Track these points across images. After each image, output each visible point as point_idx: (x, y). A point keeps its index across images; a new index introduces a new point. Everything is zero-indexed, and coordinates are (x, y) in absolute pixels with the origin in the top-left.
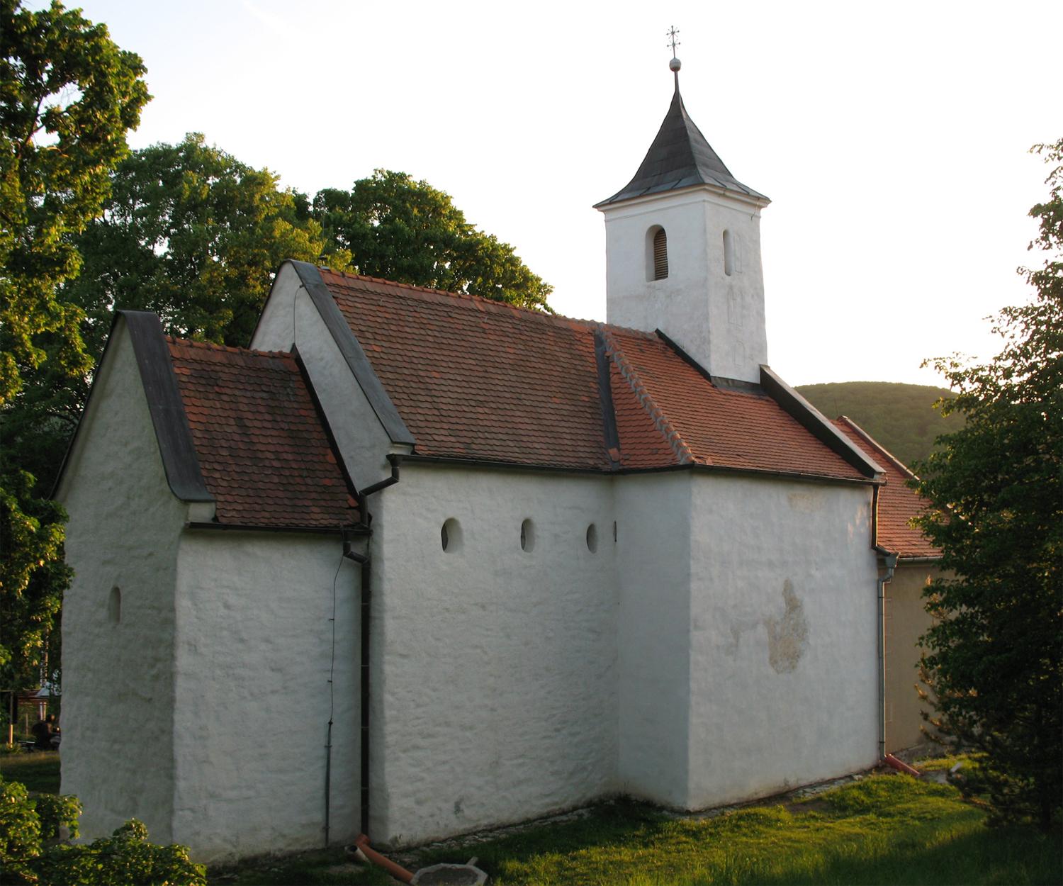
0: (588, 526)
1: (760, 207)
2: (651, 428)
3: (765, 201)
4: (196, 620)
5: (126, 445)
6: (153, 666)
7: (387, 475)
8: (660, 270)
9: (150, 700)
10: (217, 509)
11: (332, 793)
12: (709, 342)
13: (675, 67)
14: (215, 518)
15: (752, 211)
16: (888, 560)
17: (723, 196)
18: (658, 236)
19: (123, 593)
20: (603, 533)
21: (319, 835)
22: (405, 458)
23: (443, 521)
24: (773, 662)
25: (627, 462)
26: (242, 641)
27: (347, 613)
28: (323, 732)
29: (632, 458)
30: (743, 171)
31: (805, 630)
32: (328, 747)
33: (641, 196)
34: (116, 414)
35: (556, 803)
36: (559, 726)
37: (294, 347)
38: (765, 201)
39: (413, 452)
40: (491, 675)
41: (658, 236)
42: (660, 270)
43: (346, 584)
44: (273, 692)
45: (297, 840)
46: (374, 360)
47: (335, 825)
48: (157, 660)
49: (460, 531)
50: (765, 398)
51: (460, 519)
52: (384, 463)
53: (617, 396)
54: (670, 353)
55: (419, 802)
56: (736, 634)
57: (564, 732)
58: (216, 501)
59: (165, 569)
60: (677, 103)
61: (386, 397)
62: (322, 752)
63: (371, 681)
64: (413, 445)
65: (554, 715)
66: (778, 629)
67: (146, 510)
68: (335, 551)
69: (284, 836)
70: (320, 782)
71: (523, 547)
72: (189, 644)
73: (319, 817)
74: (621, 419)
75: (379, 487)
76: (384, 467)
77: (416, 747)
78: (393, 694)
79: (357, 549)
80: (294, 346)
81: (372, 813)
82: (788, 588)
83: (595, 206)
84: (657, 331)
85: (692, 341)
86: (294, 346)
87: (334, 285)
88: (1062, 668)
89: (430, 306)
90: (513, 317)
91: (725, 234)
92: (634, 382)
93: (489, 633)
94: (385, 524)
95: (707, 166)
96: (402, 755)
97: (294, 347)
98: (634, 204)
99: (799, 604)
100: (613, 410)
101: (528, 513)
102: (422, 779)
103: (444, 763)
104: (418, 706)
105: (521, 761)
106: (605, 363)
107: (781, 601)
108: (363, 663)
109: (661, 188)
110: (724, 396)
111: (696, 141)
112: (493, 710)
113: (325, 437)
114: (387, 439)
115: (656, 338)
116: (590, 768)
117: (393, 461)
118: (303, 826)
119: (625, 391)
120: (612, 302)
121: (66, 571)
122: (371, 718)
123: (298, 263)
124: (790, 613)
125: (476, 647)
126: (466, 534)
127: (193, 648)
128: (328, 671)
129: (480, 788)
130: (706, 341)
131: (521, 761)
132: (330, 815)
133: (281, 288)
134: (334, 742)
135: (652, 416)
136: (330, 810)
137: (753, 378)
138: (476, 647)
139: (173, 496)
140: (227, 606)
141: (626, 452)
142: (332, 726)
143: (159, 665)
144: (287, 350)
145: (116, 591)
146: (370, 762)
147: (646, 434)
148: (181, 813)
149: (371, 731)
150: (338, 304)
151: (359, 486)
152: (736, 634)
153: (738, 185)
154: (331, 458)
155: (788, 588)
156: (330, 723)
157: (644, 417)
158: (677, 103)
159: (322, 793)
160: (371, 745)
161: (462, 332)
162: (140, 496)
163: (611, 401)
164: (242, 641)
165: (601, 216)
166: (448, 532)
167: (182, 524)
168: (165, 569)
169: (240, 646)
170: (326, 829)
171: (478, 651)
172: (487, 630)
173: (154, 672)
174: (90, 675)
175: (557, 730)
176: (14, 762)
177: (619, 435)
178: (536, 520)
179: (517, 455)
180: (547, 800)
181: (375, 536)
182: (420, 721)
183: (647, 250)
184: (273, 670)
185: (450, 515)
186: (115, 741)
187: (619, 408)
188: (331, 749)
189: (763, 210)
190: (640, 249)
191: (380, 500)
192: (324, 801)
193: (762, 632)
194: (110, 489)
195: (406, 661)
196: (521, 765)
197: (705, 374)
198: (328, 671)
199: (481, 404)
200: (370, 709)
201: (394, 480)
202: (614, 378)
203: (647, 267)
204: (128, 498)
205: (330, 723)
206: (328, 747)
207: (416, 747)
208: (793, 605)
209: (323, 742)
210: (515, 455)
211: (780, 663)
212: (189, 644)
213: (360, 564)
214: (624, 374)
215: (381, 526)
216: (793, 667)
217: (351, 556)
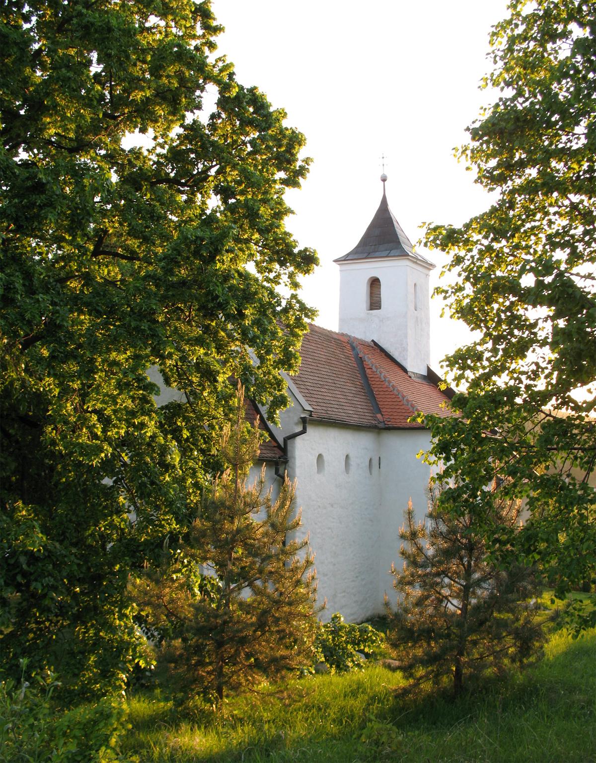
1: (430, 269)
2: (401, 404)
7: (299, 429)
8: (375, 303)
12: (407, 351)
17: (416, 263)
18: (375, 283)
25: (389, 423)
29: (392, 420)
33: (366, 258)
41: (375, 283)
42: (375, 303)
53: (373, 383)
54: (383, 354)
60: (384, 202)
64: (311, 411)
75: (294, 436)
76: (297, 424)
83: (335, 261)
85: (396, 349)
91: (415, 285)
92: (383, 374)
94: (297, 457)
100: (372, 391)
106: (360, 361)
109: (377, 254)
112: (334, 565)
114: (300, 408)
115: (372, 344)
117: (304, 421)
119: (378, 379)
120: (342, 321)
130: (405, 349)
135: (400, 396)
137: (425, 373)
158: (384, 202)
163: (369, 385)
165: (337, 267)
175: (357, 577)
181: (290, 463)
187: (376, 389)
191: (294, 443)
197: (405, 370)
199: (322, 386)
201: (304, 431)
202: (368, 371)
214: (374, 369)
215: (294, 458)
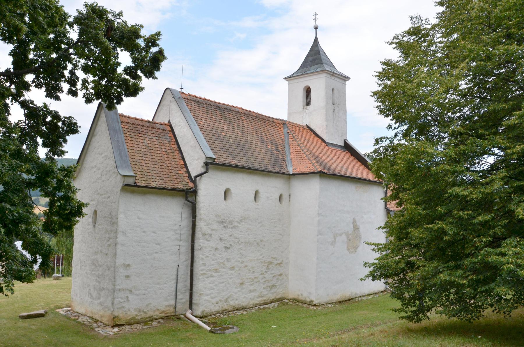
0: (280, 195)
3: (349, 78)
4: (126, 223)
5: (101, 154)
6: (108, 241)
7: (203, 170)
9: (107, 254)
11: (178, 293)
13: (316, 28)
14: (135, 183)
15: (343, 82)
16: (391, 213)
18: (308, 91)
20: (285, 197)
21: (172, 309)
22: (211, 164)
23: (225, 189)
24: (348, 249)
26: (144, 232)
27: (186, 223)
28: (176, 269)
30: (341, 68)
32: (177, 275)
35: (264, 300)
37: (169, 122)
38: (349, 78)
45: (163, 312)
46: (200, 127)
47: (179, 306)
48: (110, 238)
49: (231, 193)
51: (231, 189)
52: (203, 165)
54: (311, 133)
55: (212, 298)
56: (335, 238)
57: (268, 273)
59: (115, 202)
60: (316, 40)
61: (205, 141)
62: (175, 277)
64: (214, 159)
67: (108, 180)
68: (182, 201)
69: (158, 310)
70: (174, 289)
71: (255, 201)
72: (123, 232)
73: (173, 302)
81: (194, 302)
82: (354, 222)
83: (285, 79)
84: (306, 125)
87: (185, 98)
90: (253, 116)
91: (333, 89)
93: (241, 233)
95: (327, 64)
96: (206, 279)
97: (169, 122)
101: (257, 188)
102: (214, 289)
103: (222, 283)
111: (323, 56)
113: (180, 155)
118: (166, 306)
121: (71, 199)
126: (233, 195)
127: (124, 233)
129: (236, 293)
132: (177, 302)
133: (165, 98)
136: (177, 300)
139: (119, 175)
140: (139, 218)
143: (111, 240)
144: (166, 122)
147: (303, 161)
150: (187, 106)
152: (335, 238)
153: (338, 72)
154: (182, 163)
155: (354, 222)
156: (178, 266)
158: (316, 40)
159: (174, 293)
162: (106, 174)
164: (144, 232)
166: (226, 193)
167: (122, 185)
168: (115, 202)
169: (144, 234)
170: (175, 308)
173: (109, 243)
174: (84, 244)
178: (260, 191)
180: (261, 299)
183: (303, 95)
184: (156, 244)
185: (228, 187)
186: (93, 271)
189: (347, 82)
190: (301, 95)
192: (175, 297)
193: (344, 237)
194: (95, 172)
195: (209, 242)
196: (252, 285)
200: (194, 260)
203: (303, 101)
204: (102, 175)
205: (178, 266)
206: (177, 275)
207: (212, 276)
208: (356, 228)
209: (175, 273)
210: (255, 165)
212: (123, 232)
216: (356, 252)
217: (189, 201)
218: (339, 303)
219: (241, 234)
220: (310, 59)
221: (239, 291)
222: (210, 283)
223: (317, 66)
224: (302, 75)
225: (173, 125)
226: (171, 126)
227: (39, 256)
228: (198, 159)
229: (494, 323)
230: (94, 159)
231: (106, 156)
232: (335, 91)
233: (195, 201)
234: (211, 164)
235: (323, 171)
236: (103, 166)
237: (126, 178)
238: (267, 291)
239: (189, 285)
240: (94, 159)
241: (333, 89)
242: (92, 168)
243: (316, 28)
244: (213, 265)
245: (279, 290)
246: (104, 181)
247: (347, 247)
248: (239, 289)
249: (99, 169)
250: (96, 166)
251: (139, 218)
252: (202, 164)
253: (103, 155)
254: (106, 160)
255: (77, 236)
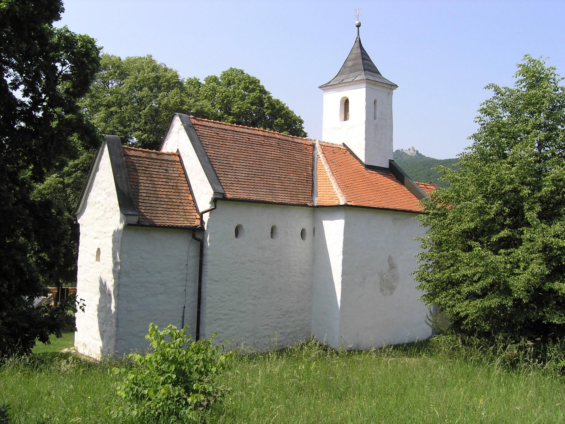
5: (105, 190)
10: (139, 218)
14: (138, 222)
18: (346, 103)
19: (101, 251)
20: (309, 232)
22: (220, 199)
24: (382, 290)
26: (148, 272)
27: (194, 262)
31: (398, 278)
32: (183, 317)
34: (101, 177)
36: (284, 313)
37: (178, 151)
38: (396, 86)
39: (223, 197)
40: (254, 290)
43: (193, 249)
44: (161, 294)
50: (390, 174)
53: (320, 173)
58: (138, 215)
62: (181, 319)
63: (202, 290)
65: (282, 309)
66: (385, 276)
71: (272, 237)
74: (320, 183)
77: (220, 319)
78: (210, 296)
79: (198, 236)
80: (178, 150)
82: (390, 258)
86: (178, 150)
88: (564, 257)
89: (238, 133)
97: (178, 151)
98: (339, 87)
99: (396, 266)
104: (222, 302)
105: (266, 327)
107: (387, 265)
108: (199, 283)
110: (370, 174)
116: (298, 332)
122: (201, 306)
123: (183, 115)
124: (390, 270)
125: (248, 278)
128: (184, 286)
131: (266, 327)
134: (186, 316)
138: (248, 278)
140: (143, 258)
141: (320, 198)
142: (185, 308)
144: (175, 151)
145: (99, 251)
146: (200, 324)
148: (120, 341)
149: (201, 311)
151: (201, 210)
155: (390, 258)
156: (184, 307)
157: (329, 183)
160: (201, 317)
161: (251, 145)
162: (109, 212)
164: (148, 272)
171: (249, 280)
172: (253, 271)
175: (284, 315)
176: (343, 198)
177: (318, 190)
179: (270, 198)
182: (222, 308)
185: (240, 223)
188: (185, 318)
198: (184, 286)
200: (201, 302)
205: (184, 307)
206: (183, 317)
207: (220, 319)
208: (392, 266)
209: (181, 315)
211: (385, 291)
213: (200, 243)
216: (392, 293)
218: (406, 350)
219: (254, 274)
220: (350, 64)
221: (251, 335)
222: (218, 327)
223: (357, 72)
224: (339, 84)
225: (182, 155)
226: (179, 156)
227: (6, 81)
228: (207, 194)
229: (96, 360)
230: (98, 194)
231: (109, 192)
232: (378, 104)
233: (203, 238)
234: (220, 199)
235: (349, 203)
236: (106, 203)
237: (129, 217)
238: (284, 336)
239: (195, 328)
240: (98, 194)
241: (375, 102)
242: (96, 204)
243: (358, 26)
244: (222, 307)
245: (299, 335)
246: (107, 218)
247: (381, 289)
248: (251, 333)
249: (102, 205)
250: (99, 202)
251: (143, 258)
252: (210, 200)
253: (107, 191)
254: (109, 196)
255: (81, 274)
